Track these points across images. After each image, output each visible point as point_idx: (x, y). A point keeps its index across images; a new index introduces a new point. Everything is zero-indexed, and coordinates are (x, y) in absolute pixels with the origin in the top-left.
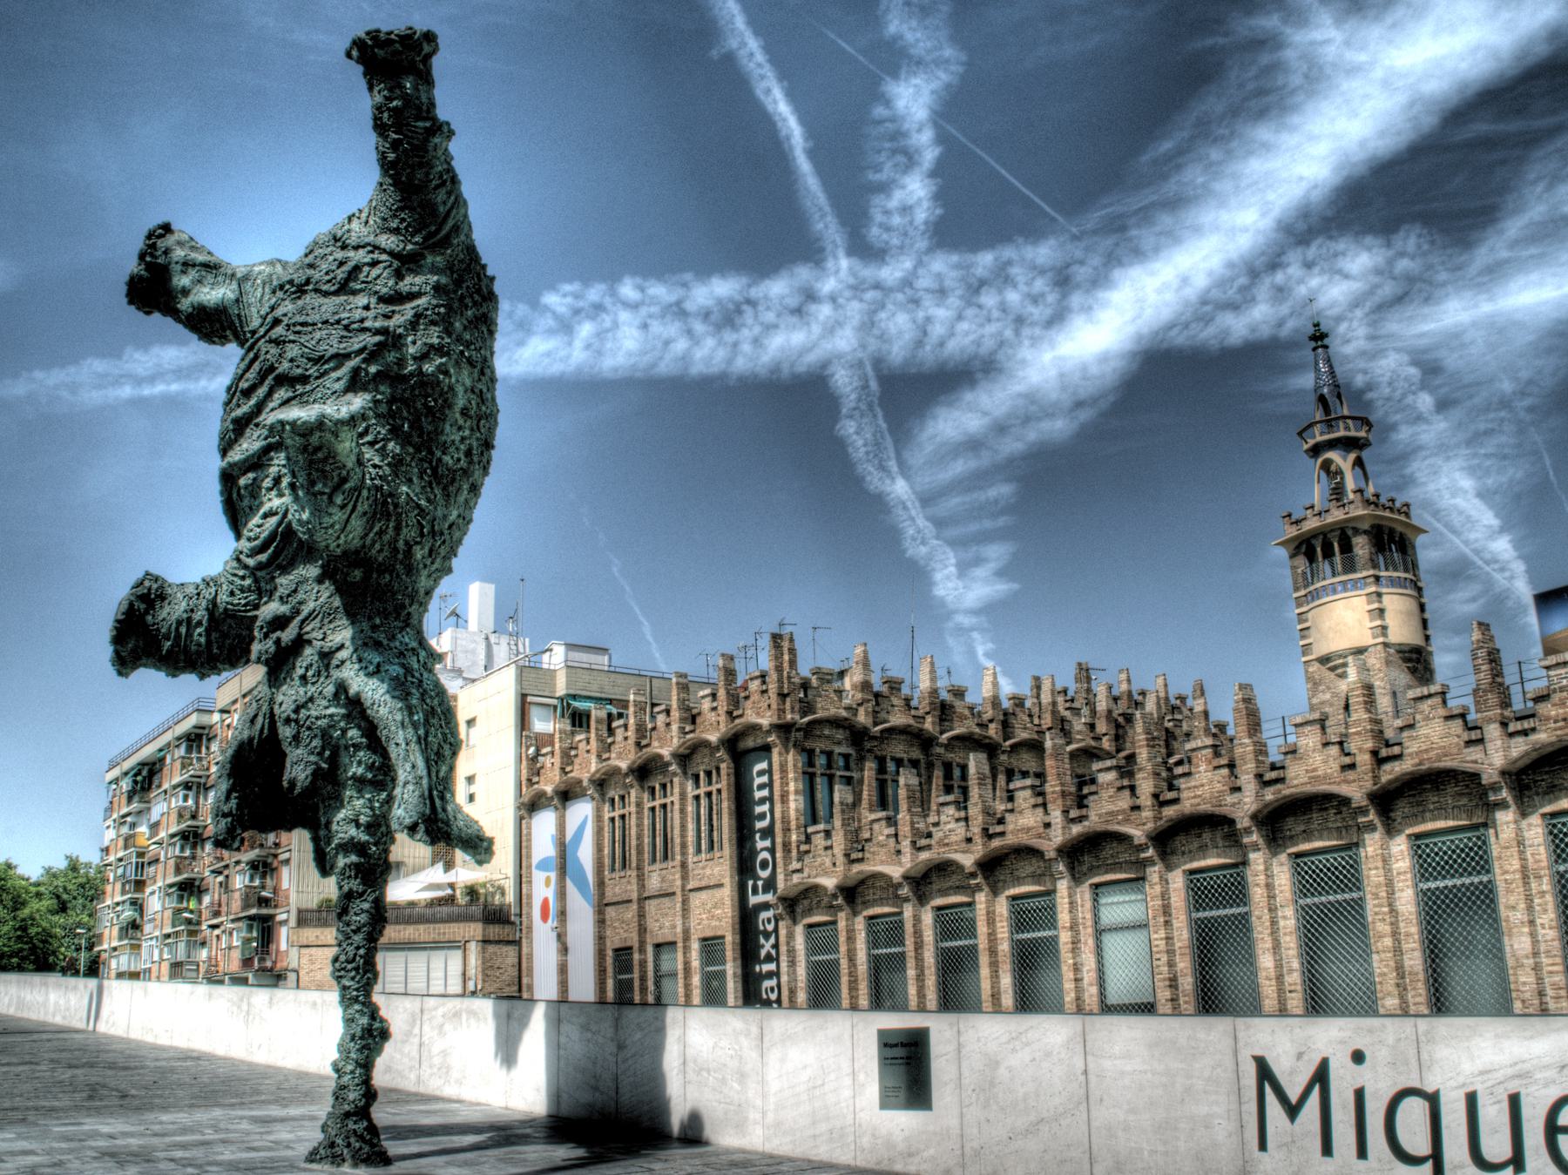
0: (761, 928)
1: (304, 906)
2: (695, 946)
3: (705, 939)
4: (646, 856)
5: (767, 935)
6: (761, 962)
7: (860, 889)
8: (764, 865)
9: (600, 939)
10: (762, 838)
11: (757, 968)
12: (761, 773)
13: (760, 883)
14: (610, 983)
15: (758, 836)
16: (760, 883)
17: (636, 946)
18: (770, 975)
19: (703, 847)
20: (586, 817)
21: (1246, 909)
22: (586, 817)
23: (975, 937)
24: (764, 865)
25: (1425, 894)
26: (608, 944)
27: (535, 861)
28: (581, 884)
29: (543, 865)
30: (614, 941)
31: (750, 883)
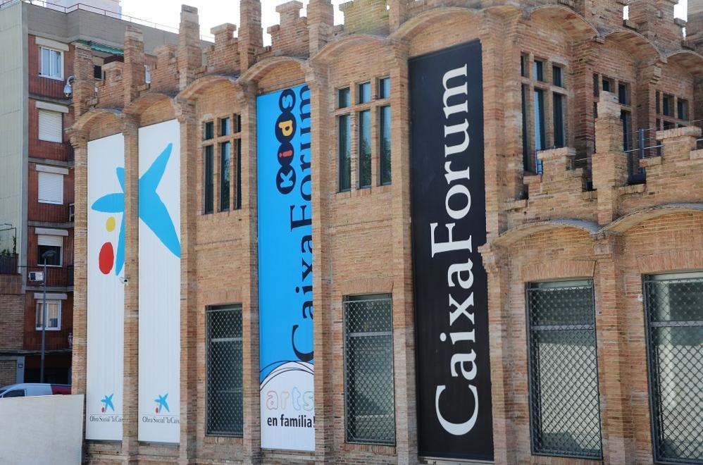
0: (451, 284)
1: (563, 100)
2: (338, 305)
3: (351, 297)
4: (231, 201)
5: (461, 295)
6: (449, 330)
7: (633, 236)
8: (458, 202)
9: (190, 294)
10: (453, 168)
11: (443, 337)
12: (454, 83)
13: (450, 226)
14: (202, 348)
15: (447, 165)
16: (450, 226)
17: (247, 303)
18: (463, 347)
19: (215, 203)
20: (170, 146)
21: (239, 339)
22: (170, 146)
23: (241, 336)
24: (458, 202)
25: (387, 327)
26: (200, 298)
27: (92, 199)
28: (164, 230)
29: (105, 204)
30: (212, 295)
31: (434, 226)
